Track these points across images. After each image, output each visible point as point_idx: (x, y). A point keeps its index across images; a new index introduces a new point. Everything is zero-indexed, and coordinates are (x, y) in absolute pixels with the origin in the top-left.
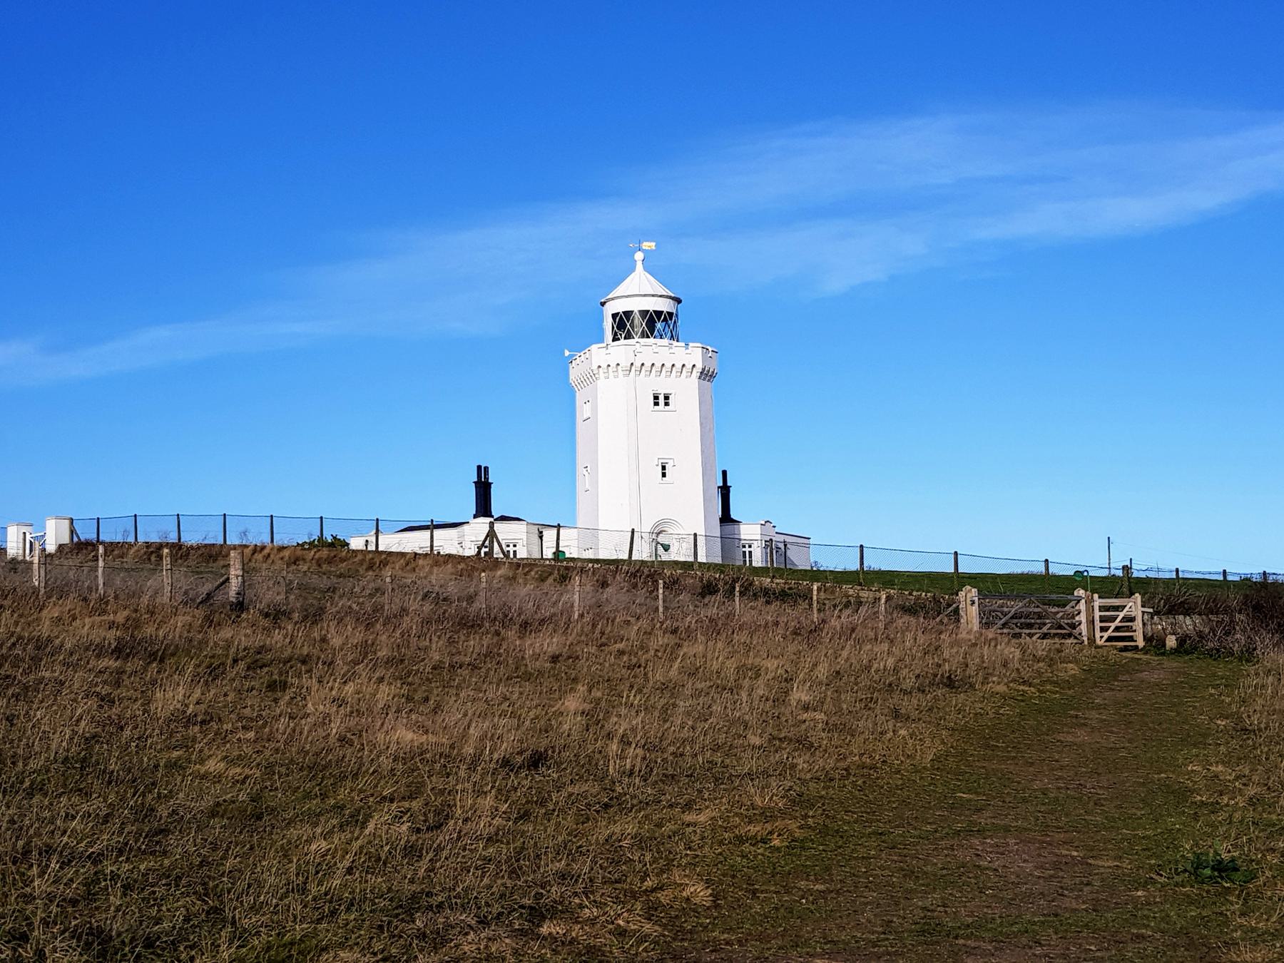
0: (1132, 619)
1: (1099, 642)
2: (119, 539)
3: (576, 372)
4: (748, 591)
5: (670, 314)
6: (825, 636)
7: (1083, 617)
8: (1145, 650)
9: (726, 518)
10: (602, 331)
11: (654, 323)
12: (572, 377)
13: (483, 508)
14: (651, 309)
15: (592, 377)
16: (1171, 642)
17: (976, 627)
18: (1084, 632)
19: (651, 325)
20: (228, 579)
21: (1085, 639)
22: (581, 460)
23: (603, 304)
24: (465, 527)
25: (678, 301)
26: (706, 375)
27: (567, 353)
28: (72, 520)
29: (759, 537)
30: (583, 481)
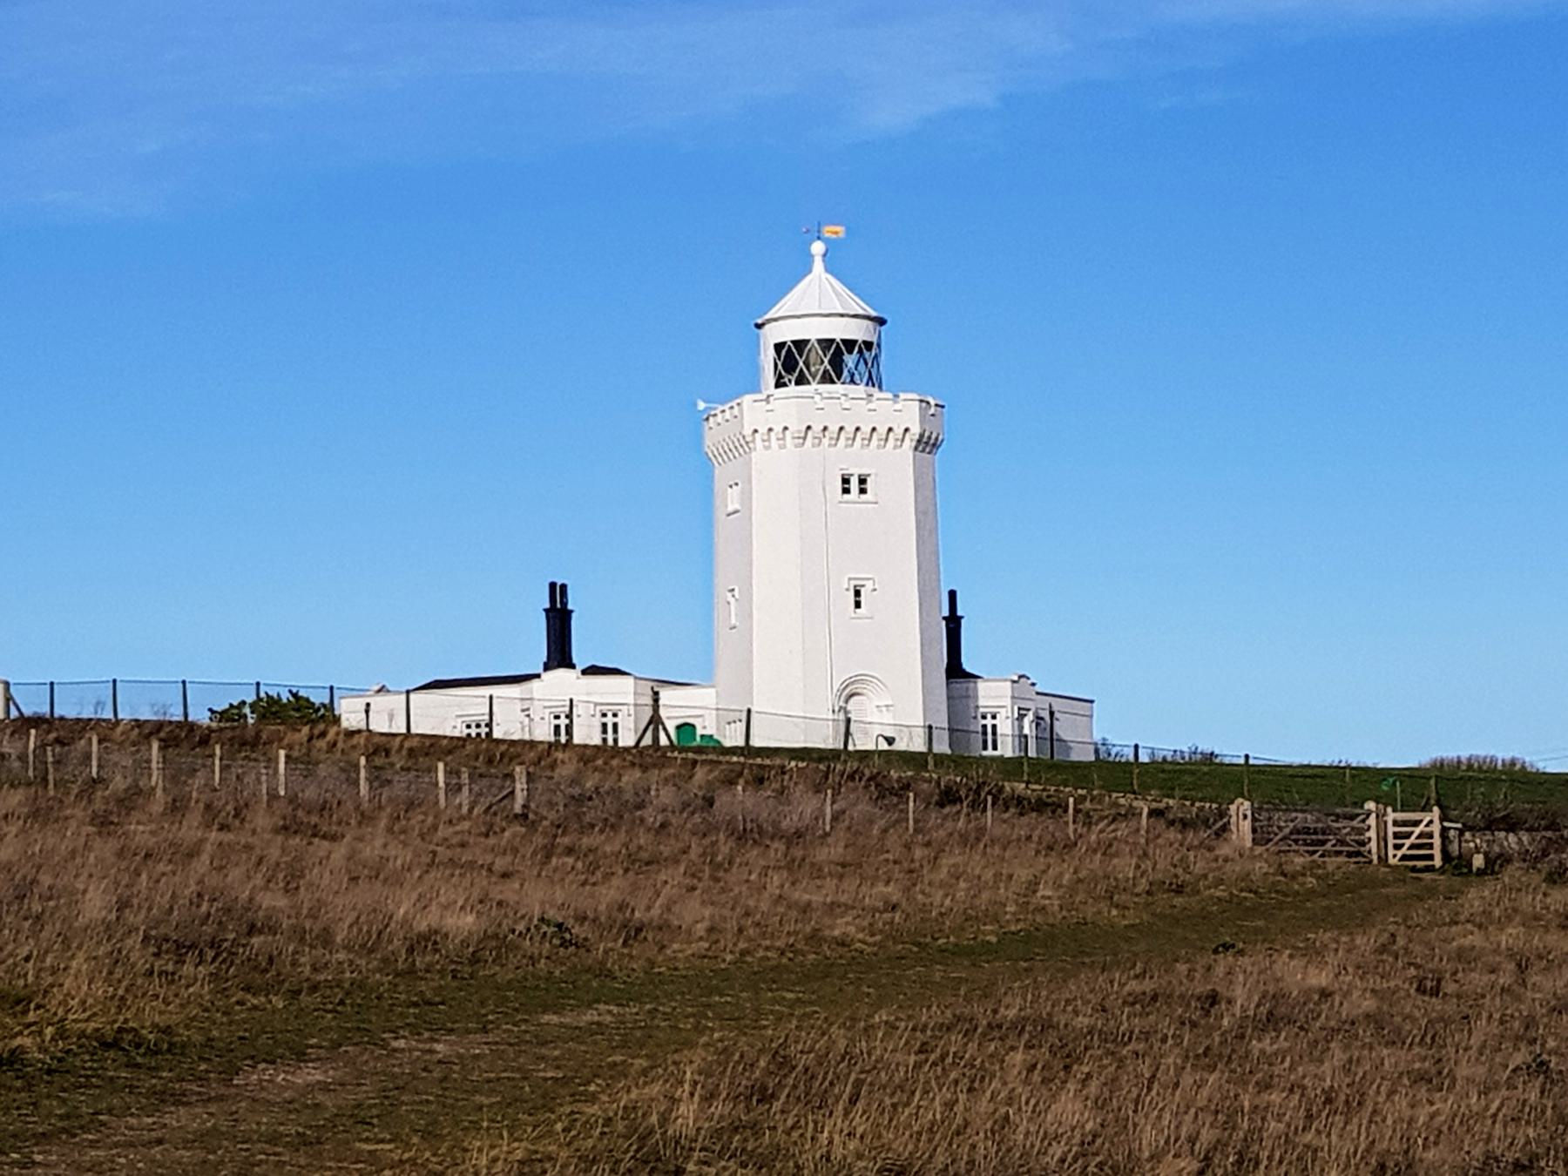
0: (1431, 836)
1: (1392, 861)
3: (714, 435)
6: (1082, 847)
7: (1372, 834)
8: (1442, 870)
9: (955, 670)
10: (757, 369)
11: (839, 360)
12: (708, 442)
13: (559, 655)
15: (743, 445)
16: (1478, 861)
17: (1249, 844)
18: (1374, 850)
20: (512, 792)
21: (1375, 858)
22: (722, 580)
23: (759, 326)
25: (881, 322)
27: (701, 405)
28: (7, 684)
29: (1008, 702)
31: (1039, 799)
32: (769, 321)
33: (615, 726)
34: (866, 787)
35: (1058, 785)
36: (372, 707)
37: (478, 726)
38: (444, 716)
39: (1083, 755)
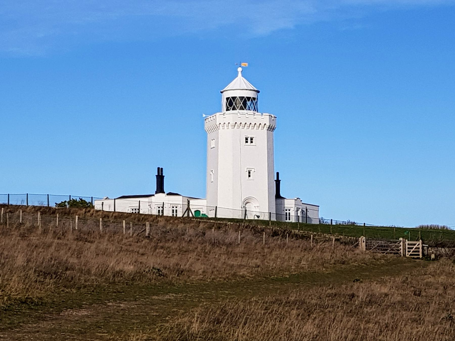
0: (419, 248)
1: (407, 256)
2: (19, 204)
3: (208, 125)
4: (292, 236)
5: (254, 99)
7: (401, 247)
8: (422, 259)
9: (278, 196)
10: (221, 105)
11: (245, 103)
12: (206, 126)
13: (160, 189)
14: (245, 96)
15: (216, 128)
16: (433, 256)
17: (364, 250)
18: (402, 252)
19: (245, 104)
20: (145, 230)
23: (222, 92)
24: (153, 197)
26: (271, 129)
27: (204, 116)
29: (293, 206)
31: (302, 235)
33: (176, 210)
34: (251, 230)
36: (104, 203)
37: (135, 210)
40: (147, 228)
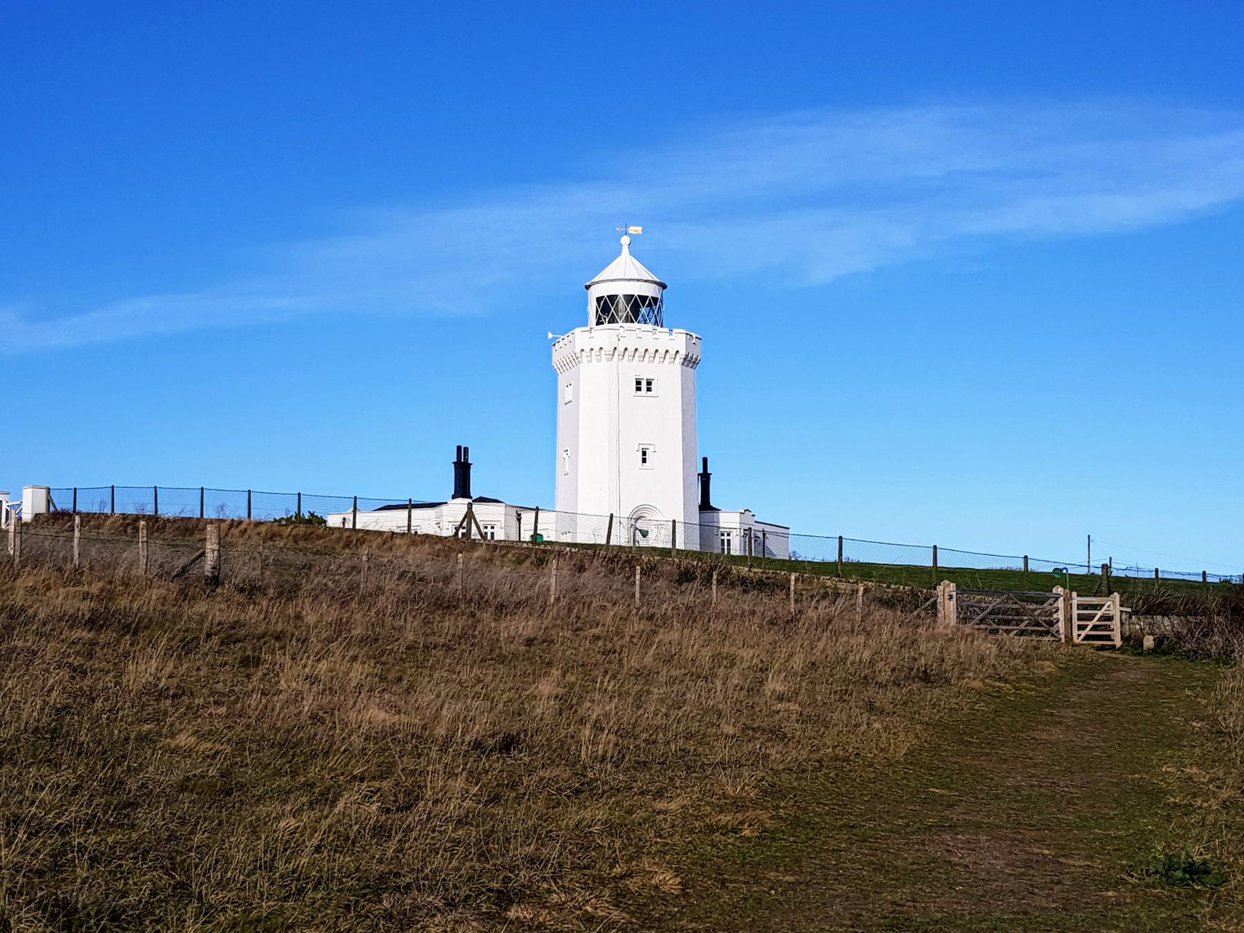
0: (1110, 618)
1: (1076, 640)
2: (96, 510)
3: (558, 355)
5: (655, 300)
7: (1060, 615)
8: (1122, 650)
9: (705, 506)
10: (586, 314)
12: (554, 360)
13: (462, 489)
14: (636, 293)
15: (575, 360)
16: (1149, 642)
18: (1062, 630)
19: (635, 310)
21: (1063, 637)
22: (562, 443)
23: (588, 287)
24: (444, 507)
25: (664, 286)
26: (690, 362)
28: (49, 489)
29: (738, 526)
30: (563, 465)
31: (761, 580)
32: (594, 283)
34: (622, 568)
35: (762, 576)
38: (394, 521)
39: (780, 555)
40: (209, 546)
